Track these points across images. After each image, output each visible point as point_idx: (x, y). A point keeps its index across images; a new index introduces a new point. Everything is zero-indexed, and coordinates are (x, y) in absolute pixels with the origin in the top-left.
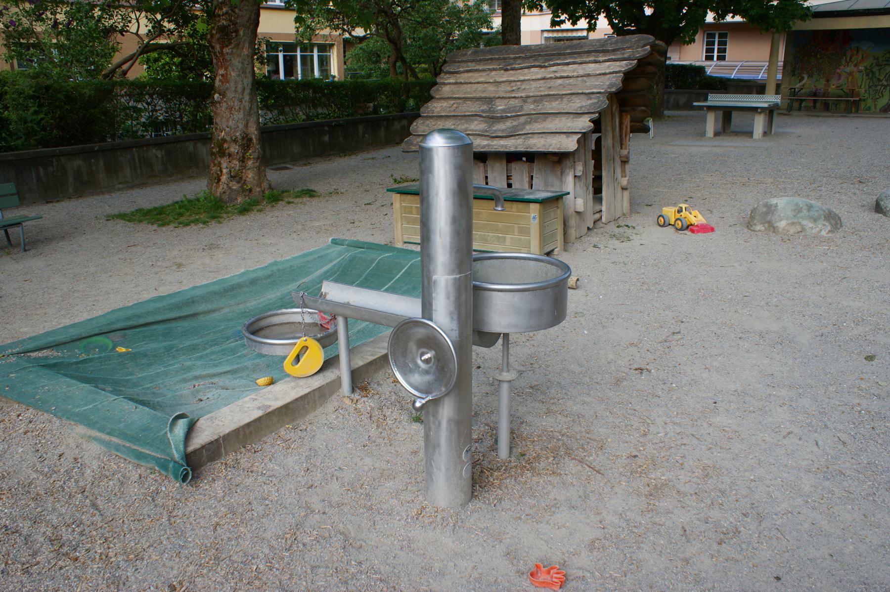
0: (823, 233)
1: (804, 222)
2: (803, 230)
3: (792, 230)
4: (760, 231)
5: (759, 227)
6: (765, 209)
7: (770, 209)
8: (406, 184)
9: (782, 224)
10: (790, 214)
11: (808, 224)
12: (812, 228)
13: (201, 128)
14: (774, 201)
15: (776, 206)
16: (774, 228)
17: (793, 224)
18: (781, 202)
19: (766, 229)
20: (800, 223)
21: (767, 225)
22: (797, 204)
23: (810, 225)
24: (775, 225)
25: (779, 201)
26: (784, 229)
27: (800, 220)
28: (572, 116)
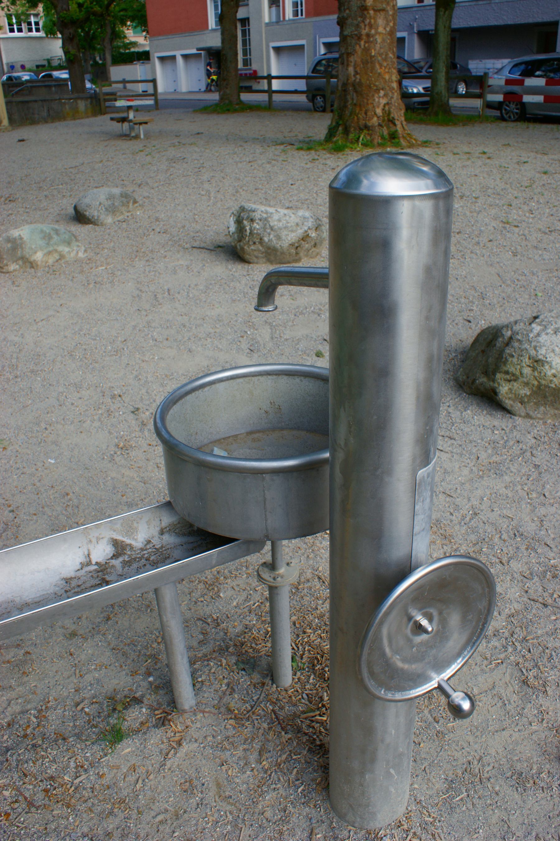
0: (81, 255)
1: (60, 248)
2: (62, 257)
3: (51, 261)
4: (15, 270)
5: (13, 267)
6: (9, 245)
7: (16, 245)
8: (178, 392)
9: (39, 256)
10: (41, 243)
11: (64, 249)
12: (69, 252)
13: (173, 703)
14: (15, 233)
15: (21, 238)
16: (31, 263)
17: (50, 253)
18: (23, 232)
19: (21, 267)
20: (56, 251)
21: (20, 262)
22: (42, 231)
23: (67, 249)
24: (32, 259)
25: (21, 233)
26: (42, 262)
27: (56, 247)
28: (304, 114)
